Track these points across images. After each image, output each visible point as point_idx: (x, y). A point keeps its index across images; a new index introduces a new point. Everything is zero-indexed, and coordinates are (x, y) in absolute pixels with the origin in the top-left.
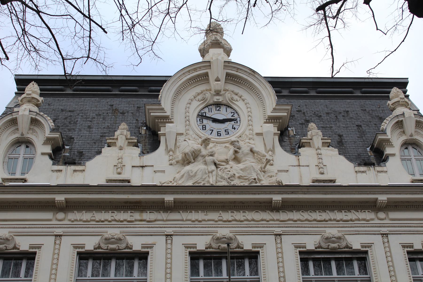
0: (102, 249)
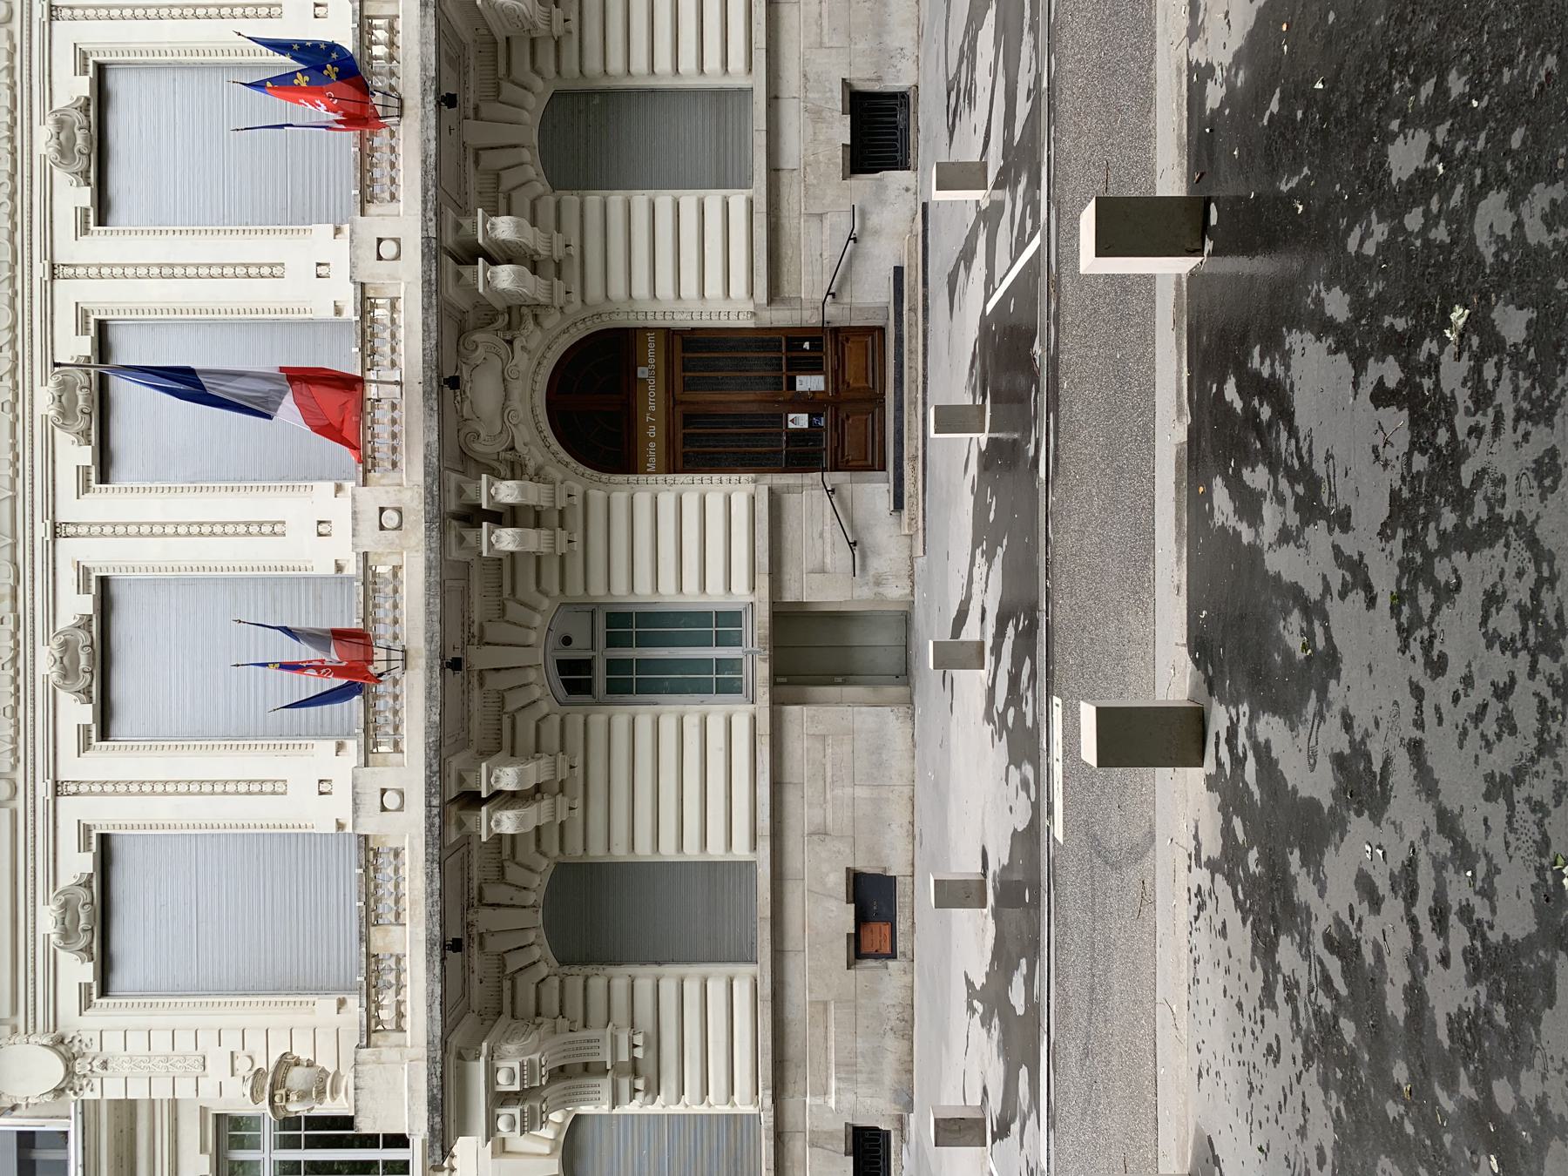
0: (90, 685)
